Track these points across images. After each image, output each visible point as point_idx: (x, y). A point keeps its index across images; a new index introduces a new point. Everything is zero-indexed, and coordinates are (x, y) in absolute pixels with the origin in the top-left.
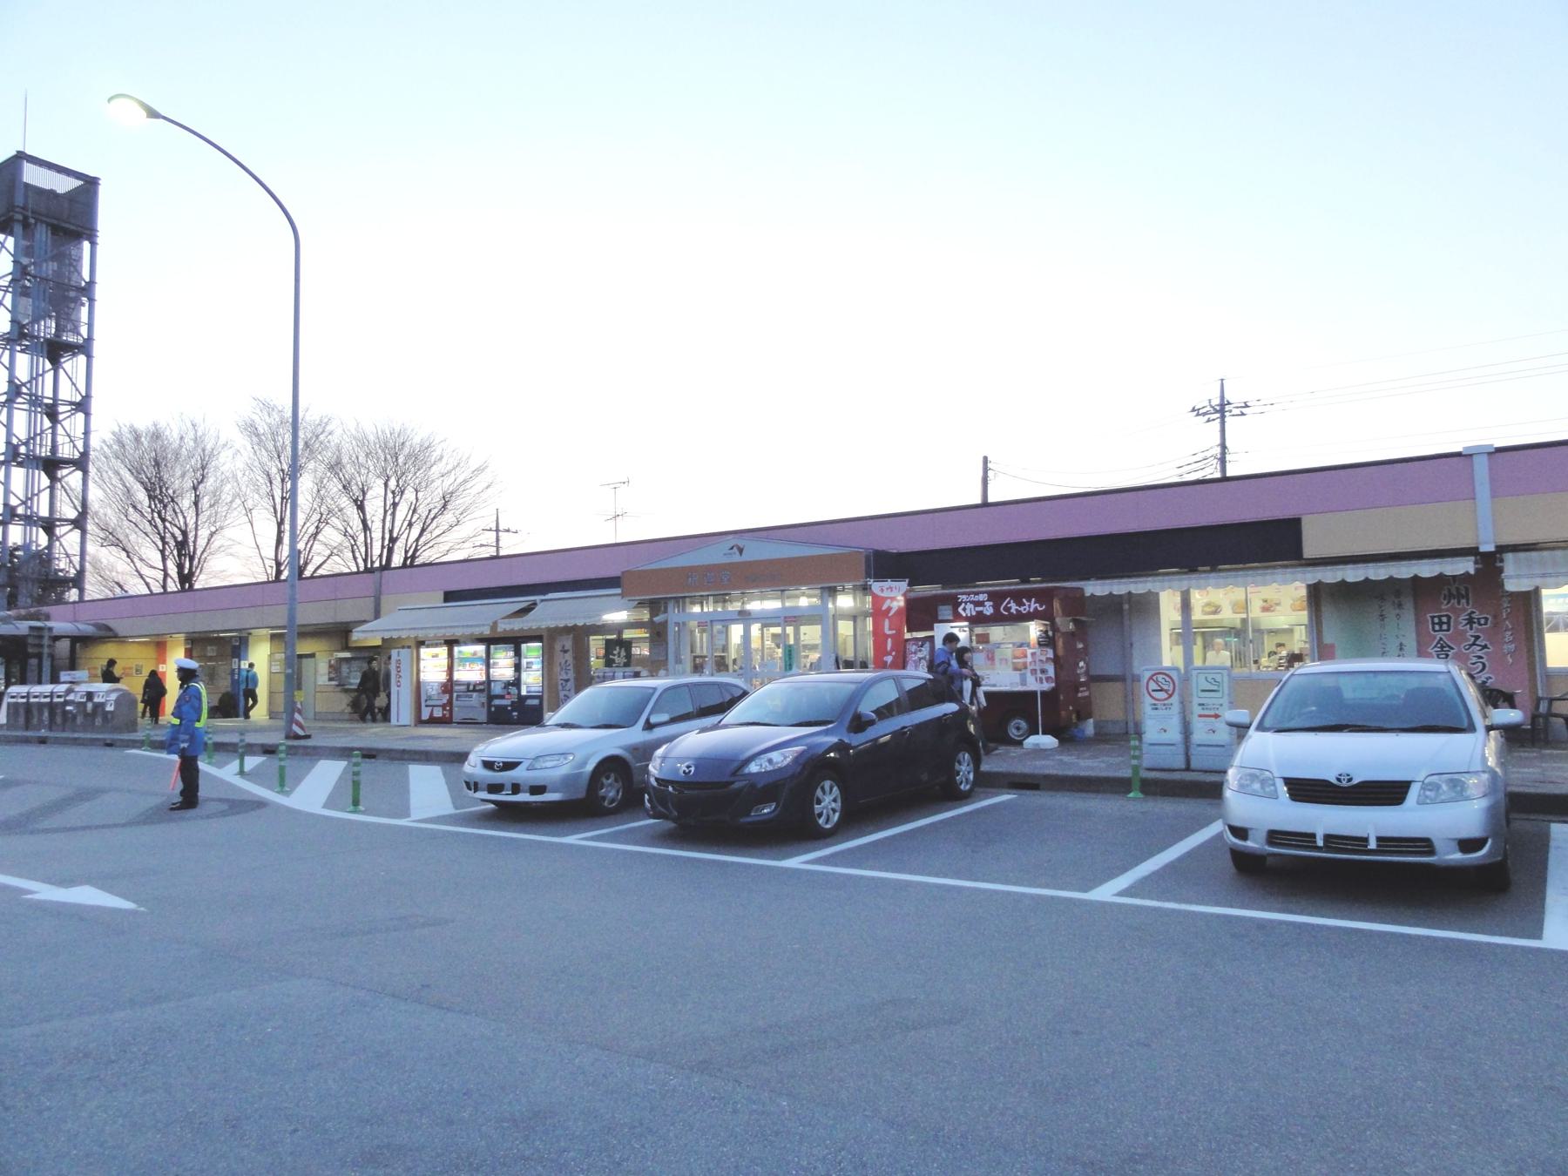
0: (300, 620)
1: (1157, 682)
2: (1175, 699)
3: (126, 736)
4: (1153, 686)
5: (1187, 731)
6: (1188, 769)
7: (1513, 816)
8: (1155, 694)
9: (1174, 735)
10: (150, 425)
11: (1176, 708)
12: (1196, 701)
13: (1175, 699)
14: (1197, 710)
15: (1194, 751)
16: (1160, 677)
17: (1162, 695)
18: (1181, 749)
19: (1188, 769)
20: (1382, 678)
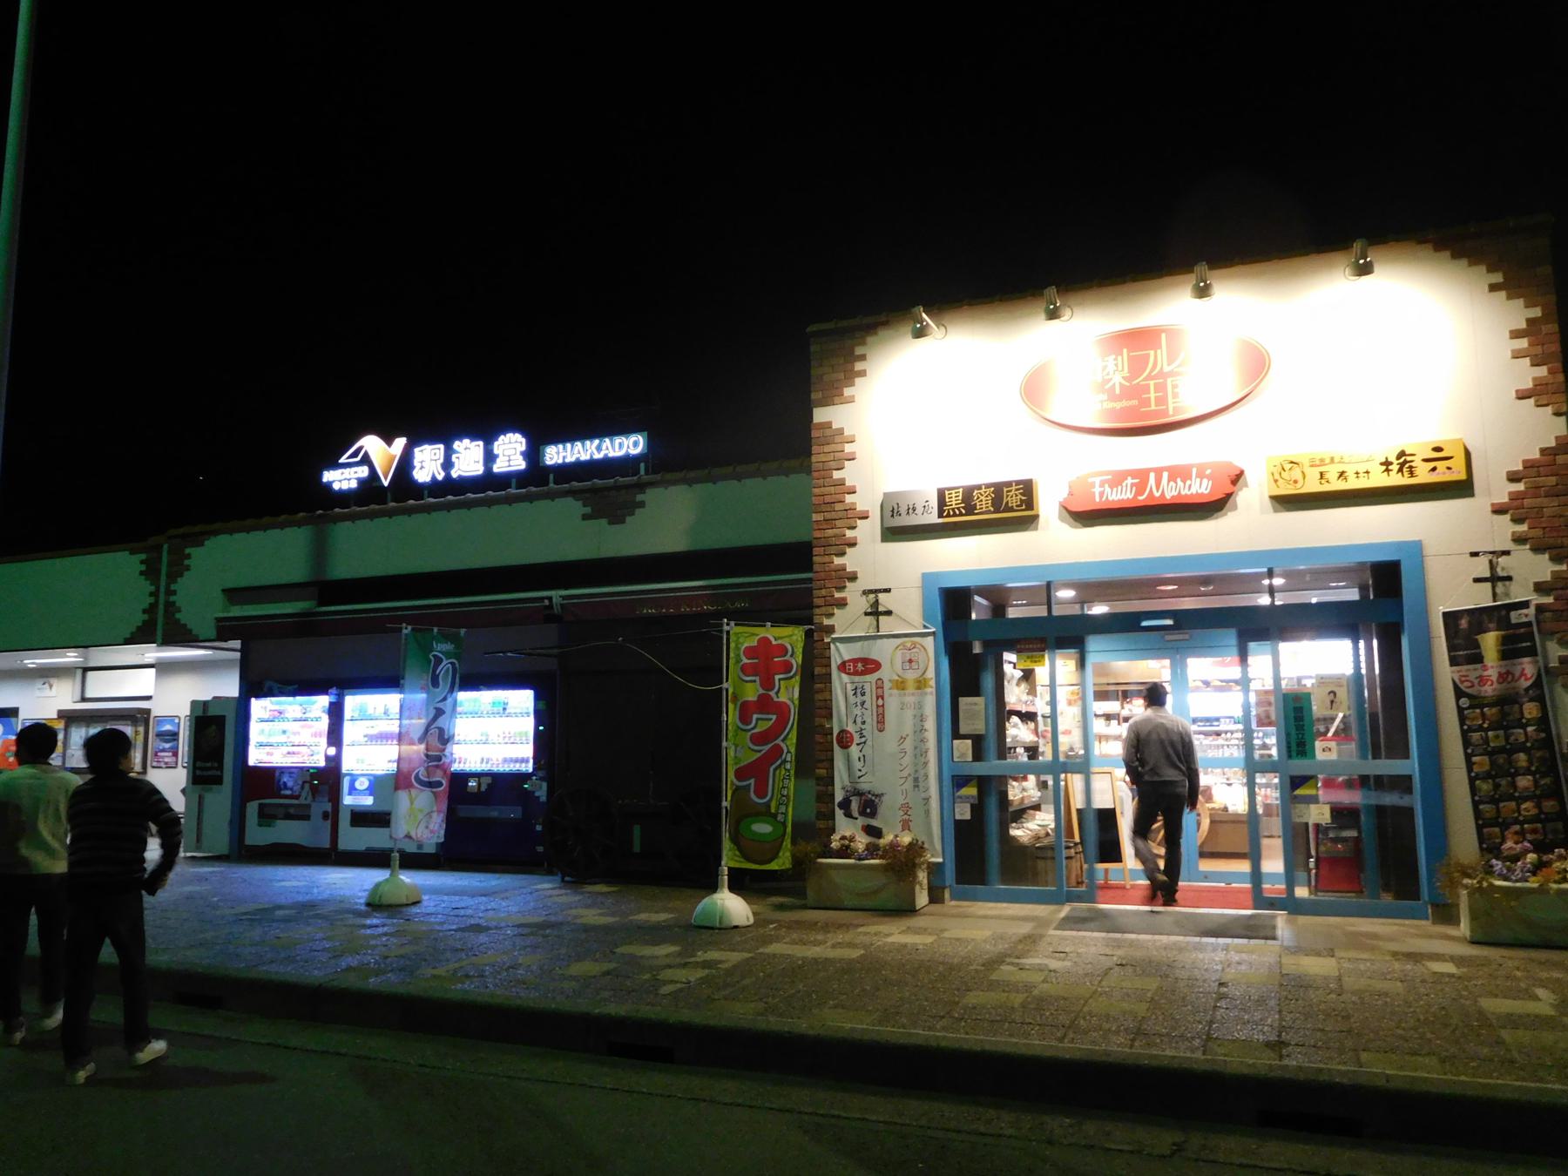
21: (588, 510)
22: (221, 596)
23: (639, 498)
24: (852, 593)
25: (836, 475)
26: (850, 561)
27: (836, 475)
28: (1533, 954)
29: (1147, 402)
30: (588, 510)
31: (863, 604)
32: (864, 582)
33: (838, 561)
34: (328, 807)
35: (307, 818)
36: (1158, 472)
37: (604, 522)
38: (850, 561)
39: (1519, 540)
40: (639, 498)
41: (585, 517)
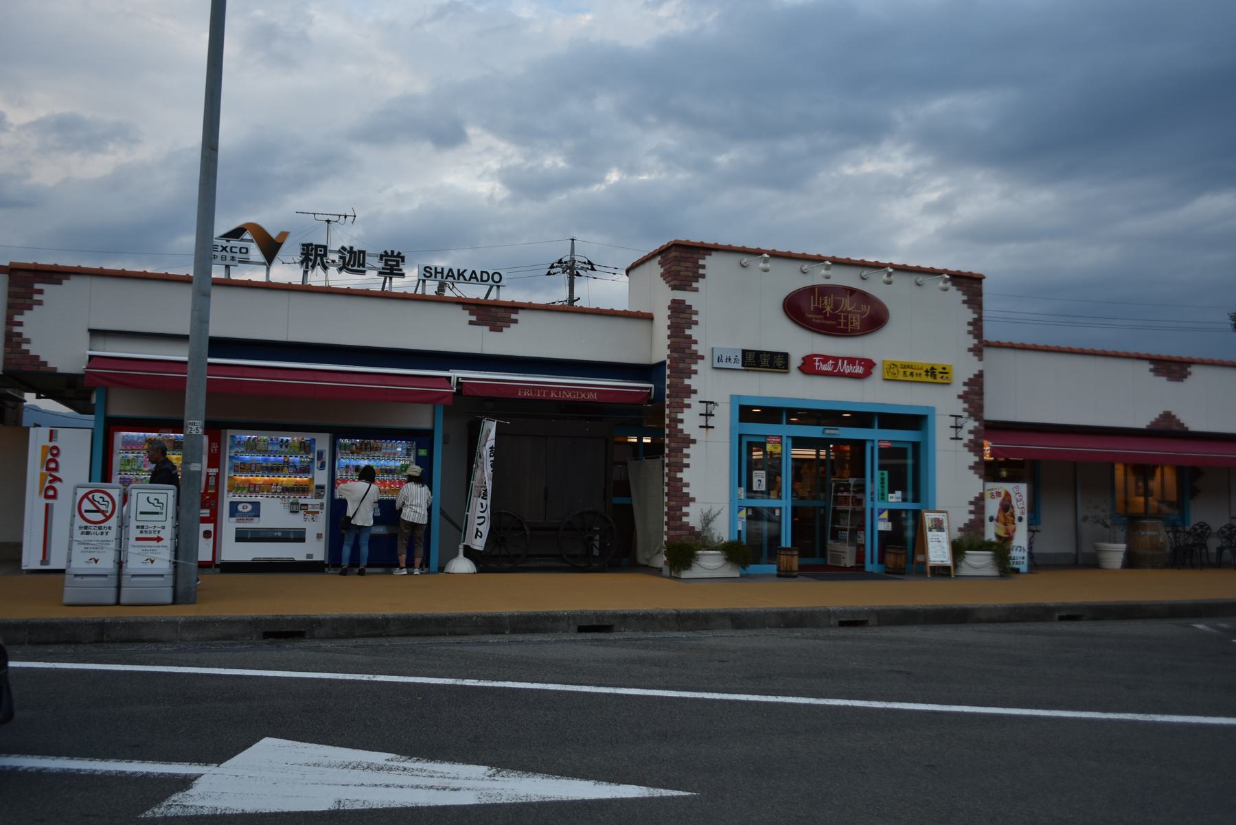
0: (218, 329)
1: (92, 501)
2: (113, 522)
3: (810, 453)
4: (87, 505)
5: (120, 564)
6: (118, 603)
7: (655, 347)
8: (89, 516)
9: (107, 563)
10: (691, 491)
11: (113, 534)
12: (133, 524)
13: (113, 522)
14: (134, 533)
15: (125, 580)
16: (97, 496)
17: (99, 517)
18: (113, 581)
19: (118, 603)
20: (86, 579)
21: (474, 318)
22: (87, 335)
23: (513, 316)
24: (693, 400)
25: (688, 332)
26: (692, 382)
27: (688, 332)
28: (1003, 627)
29: (839, 324)
30: (474, 318)
31: (702, 408)
32: (700, 396)
33: (687, 382)
34: (806, 466)
35: (303, 540)
36: (843, 359)
37: (487, 328)
38: (692, 382)
39: (965, 410)
40: (513, 316)
41: (471, 323)
